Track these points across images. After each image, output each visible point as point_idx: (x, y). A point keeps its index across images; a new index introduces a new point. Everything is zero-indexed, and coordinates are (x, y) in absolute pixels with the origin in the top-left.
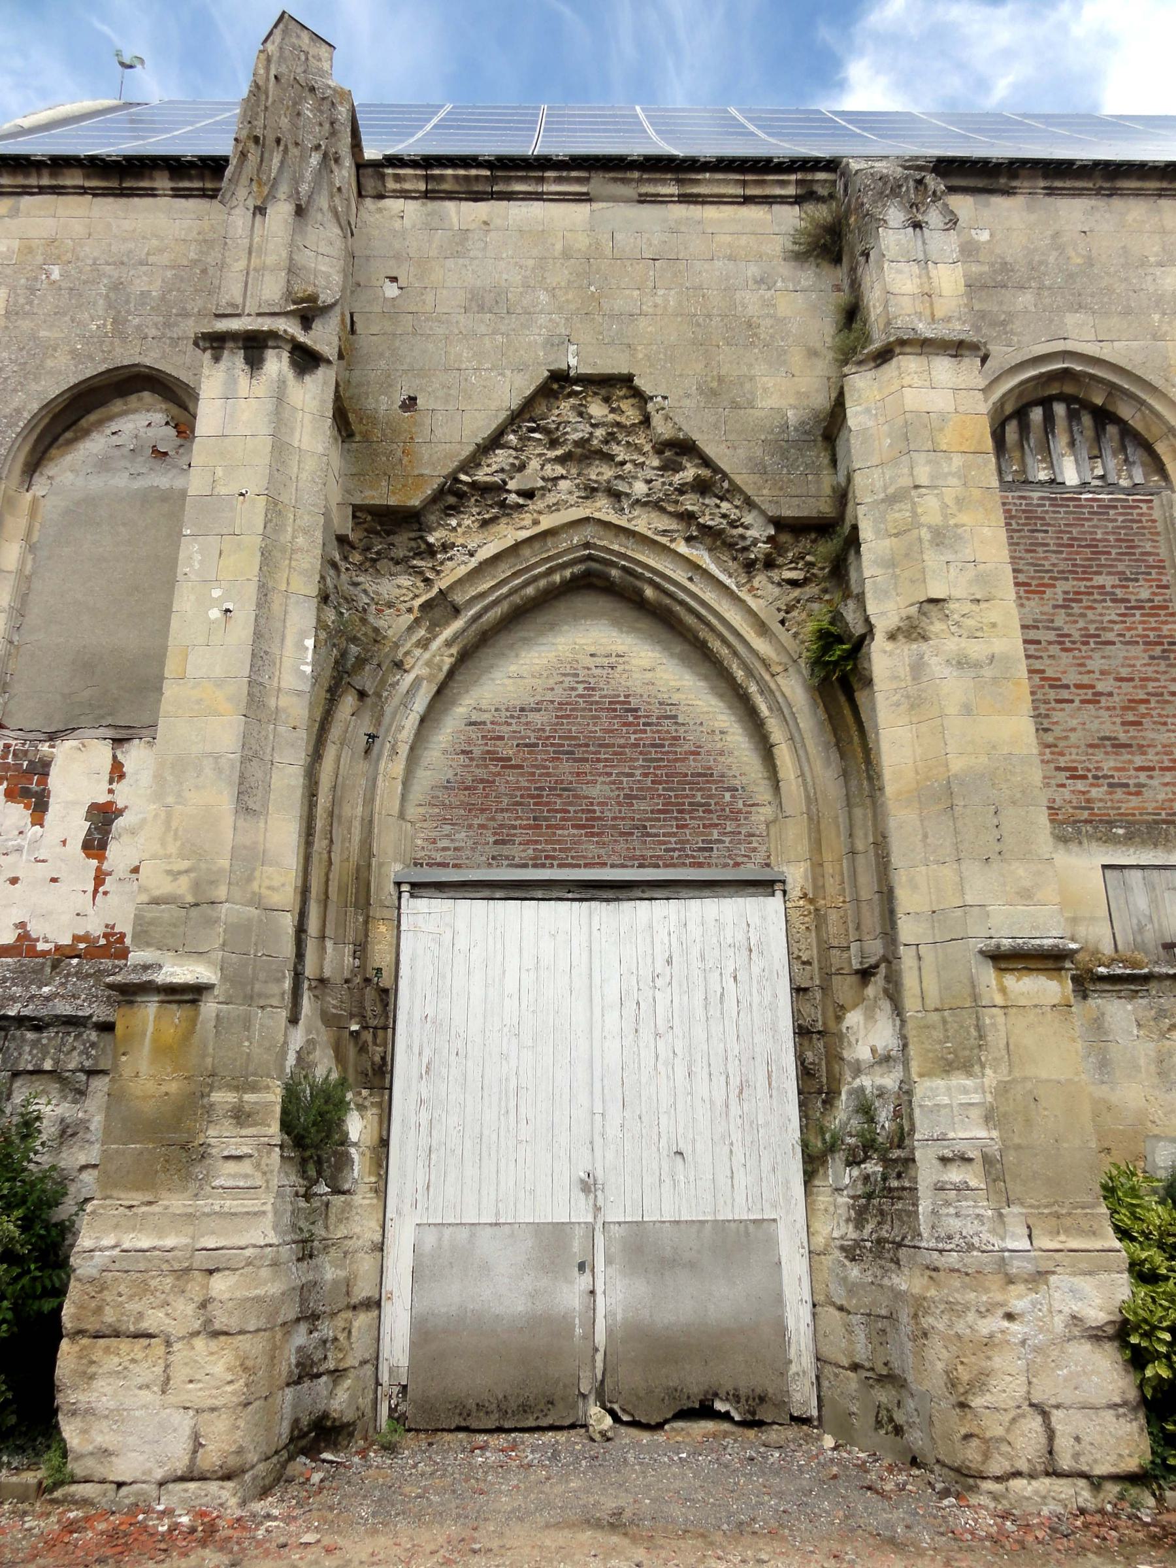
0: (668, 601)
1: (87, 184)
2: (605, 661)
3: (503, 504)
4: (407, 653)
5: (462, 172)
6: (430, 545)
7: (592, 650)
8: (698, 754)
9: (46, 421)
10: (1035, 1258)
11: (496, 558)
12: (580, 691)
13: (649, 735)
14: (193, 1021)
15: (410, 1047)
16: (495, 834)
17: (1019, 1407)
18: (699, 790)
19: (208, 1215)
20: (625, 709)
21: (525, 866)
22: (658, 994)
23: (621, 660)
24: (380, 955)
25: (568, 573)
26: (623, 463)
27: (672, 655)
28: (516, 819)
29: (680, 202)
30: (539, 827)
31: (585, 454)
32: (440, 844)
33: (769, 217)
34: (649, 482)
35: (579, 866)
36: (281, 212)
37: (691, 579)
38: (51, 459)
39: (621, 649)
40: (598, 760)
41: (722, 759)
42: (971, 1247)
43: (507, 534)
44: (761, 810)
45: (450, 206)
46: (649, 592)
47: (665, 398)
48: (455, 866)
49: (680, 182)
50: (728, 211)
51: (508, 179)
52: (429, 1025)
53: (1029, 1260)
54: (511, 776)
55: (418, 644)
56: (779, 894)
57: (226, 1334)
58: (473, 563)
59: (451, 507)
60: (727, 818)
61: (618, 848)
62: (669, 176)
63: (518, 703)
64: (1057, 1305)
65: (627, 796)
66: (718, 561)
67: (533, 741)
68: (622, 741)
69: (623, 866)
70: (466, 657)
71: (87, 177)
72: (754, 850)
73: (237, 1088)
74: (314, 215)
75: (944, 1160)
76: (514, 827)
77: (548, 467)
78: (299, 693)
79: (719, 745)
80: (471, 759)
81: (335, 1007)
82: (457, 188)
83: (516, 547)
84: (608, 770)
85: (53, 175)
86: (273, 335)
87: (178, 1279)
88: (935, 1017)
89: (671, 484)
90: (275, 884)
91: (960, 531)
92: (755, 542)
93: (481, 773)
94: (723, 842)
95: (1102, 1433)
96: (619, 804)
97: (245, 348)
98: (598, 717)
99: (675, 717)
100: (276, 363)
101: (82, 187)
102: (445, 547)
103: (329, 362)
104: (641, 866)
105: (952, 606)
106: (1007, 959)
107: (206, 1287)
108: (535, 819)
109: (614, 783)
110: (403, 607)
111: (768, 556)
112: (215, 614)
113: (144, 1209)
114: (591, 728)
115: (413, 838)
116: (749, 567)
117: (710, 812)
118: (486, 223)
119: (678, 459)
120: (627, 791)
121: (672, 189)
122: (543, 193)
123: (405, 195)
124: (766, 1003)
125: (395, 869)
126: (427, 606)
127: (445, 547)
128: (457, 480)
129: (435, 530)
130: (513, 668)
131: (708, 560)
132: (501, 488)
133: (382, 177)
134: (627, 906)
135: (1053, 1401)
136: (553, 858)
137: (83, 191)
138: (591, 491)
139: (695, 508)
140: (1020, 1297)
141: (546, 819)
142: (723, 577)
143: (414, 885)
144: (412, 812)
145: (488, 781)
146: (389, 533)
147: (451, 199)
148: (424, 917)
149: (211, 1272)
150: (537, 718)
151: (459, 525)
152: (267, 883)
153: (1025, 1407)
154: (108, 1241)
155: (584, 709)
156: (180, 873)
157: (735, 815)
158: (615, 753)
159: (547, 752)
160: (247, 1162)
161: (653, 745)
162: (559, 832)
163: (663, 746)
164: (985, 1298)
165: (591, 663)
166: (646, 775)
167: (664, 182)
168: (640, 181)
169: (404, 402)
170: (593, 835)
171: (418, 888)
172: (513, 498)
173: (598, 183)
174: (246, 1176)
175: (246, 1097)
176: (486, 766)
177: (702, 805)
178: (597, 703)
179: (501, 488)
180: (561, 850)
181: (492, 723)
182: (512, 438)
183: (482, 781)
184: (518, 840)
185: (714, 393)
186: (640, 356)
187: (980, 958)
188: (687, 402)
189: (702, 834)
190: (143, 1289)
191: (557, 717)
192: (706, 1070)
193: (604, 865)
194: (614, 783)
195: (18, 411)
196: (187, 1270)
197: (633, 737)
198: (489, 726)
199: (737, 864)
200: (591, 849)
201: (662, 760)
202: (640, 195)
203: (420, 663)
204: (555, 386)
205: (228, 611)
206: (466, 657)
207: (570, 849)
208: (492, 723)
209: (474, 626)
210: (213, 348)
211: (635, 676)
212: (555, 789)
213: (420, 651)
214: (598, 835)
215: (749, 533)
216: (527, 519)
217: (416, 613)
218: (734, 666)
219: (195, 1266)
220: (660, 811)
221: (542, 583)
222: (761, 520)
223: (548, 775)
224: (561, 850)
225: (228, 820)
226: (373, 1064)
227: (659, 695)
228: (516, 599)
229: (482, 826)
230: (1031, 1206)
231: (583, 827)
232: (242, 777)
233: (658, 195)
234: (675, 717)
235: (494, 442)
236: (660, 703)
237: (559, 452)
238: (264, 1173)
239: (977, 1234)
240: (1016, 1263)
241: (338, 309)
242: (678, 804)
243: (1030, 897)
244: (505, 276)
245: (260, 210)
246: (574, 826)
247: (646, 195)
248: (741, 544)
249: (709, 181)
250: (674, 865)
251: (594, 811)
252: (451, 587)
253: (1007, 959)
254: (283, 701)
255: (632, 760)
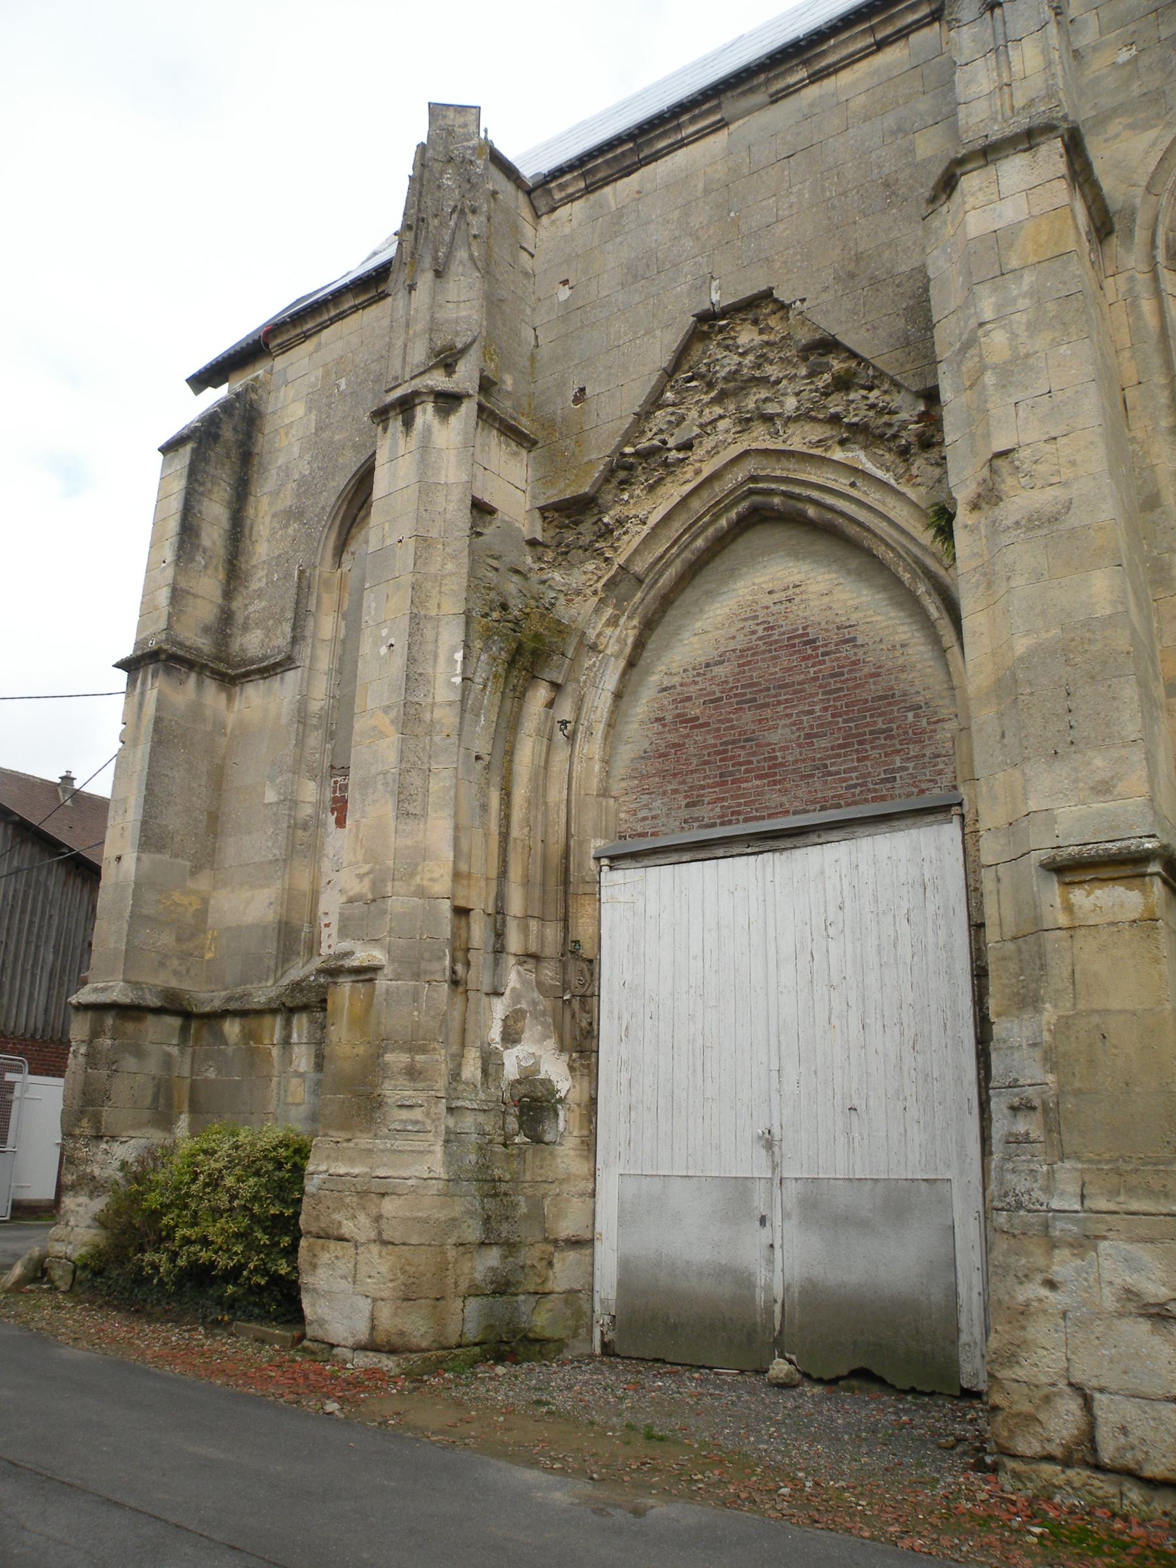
0: (829, 516)
1: (357, 302)
2: (781, 596)
3: (666, 464)
4: (599, 635)
5: (610, 156)
6: (606, 525)
7: (770, 587)
8: (878, 675)
9: (344, 507)
10: (1085, 1220)
11: (667, 518)
12: (760, 634)
13: (829, 664)
14: (371, 995)
15: (611, 1012)
16: (686, 797)
17: (1053, 1385)
18: (880, 715)
19: (382, 1151)
20: (803, 643)
21: (713, 825)
22: (832, 943)
23: (797, 590)
24: (582, 930)
25: (733, 514)
26: (778, 382)
27: (849, 572)
28: (705, 778)
29: (812, 82)
30: (724, 783)
31: (738, 385)
32: (640, 815)
33: (906, 52)
34: (797, 394)
35: (763, 818)
36: (425, 280)
37: (853, 485)
38: (353, 538)
39: (796, 578)
40: (779, 703)
41: (903, 676)
42: (1019, 1206)
43: (673, 492)
44: (947, 725)
45: (608, 190)
46: (811, 512)
47: (803, 300)
48: (653, 834)
49: (806, 63)
50: (862, 67)
51: (650, 142)
52: (626, 991)
53: (1076, 1222)
54: (698, 736)
55: (609, 623)
56: (956, 819)
57: (393, 1244)
58: (646, 529)
59: (622, 482)
60: (909, 741)
61: (800, 793)
62: (794, 62)
63: (702, 659)
64: (1106, 1276)
65: (808, 736)
66: (874, 458)
67: (718, 695)
68: (802, 677)
69: (806, 811)
70: (649, 626)
71: (356, 296)
72: (940, 772)
73: (410, 1050)
74: (456, 268)
75: (1014, 1109)
76: (703, 787)
77: (707, 411)
78: (451, 704)
79: (900, 661)
80: (664, 726)
81: (552, 979)
82: (609, 172)
83: (685, 500)
84: (789, 711)
85: (336, 305)
86: (416, 394)
87: (361, 1198)
88: (1011, 946)
89: (816, 391)
90: (435, 875)
91: (1031, 361)
92: (904, 425)
93: (672, 738)
94: (906, 769)
95: (1156, 1429)
96: (800, 746)
97: (402, 412)
98: (777, 657)
99: (854, 639)
100: (425, 414)
101: (355, 306)
102: (620, 522)
103: (469, 396)
104: (823, 809)
105: (1024, 454)
106: (1069, 869)
107: (379, 1206)
108: (721, 775)
109: (794, 724)
110: (589, 592)
111: (920, 436)
112: (384, 650)
113: (345, 1144)
114: (773, 670)
115: (617, 812)
116: (904, 453)
117: (891, 737)
118: (639, 192)
119: (824, 359)
120: (807, 731)
121: (802, 73)
122: (683, 139)
123: (571, 199)
124: (941, 944)
125: (596, 844)
126: (611, 584)
127: (620, 522)
128: (623, 455)
129: (610, 508)
130: (698, 624)
131: (864, 460)
132: (664, 446)
133: (549, 191)
134: (798, 854)
135: (1094, 1383)
136: (739, 813)
137: (356, 309)
138: (745, 423)
139: (839, 409)
140: (1063, 1263)
141: (732, 774)
142: (880, 474)
143: (612, 858)
144: (617, 787)
145: (678, 745)
146: (577, 523)
147: (607, 184)
148: (619, 886)
149: (383, 1195)
150: (719, 671)
151: (631, 497)
152: (428, 875)
153: (1062, 1385)
154: (322, 1168)
155: (764, 652)
156: (364, 875)
157: (918, 736)
158: (795, 692)
159: (731, 704)
160: (418, 1111)
161: (833, 676)
162: (744, 785)
163: (842, 674)
164: (1023, 1262)
165: (768, 600)
166: (825, 709)
167: (790, 71)
168: (768, 81)
169: (575, 396)
170: (775, 783)
171: (615, 860)
172: (674, 455)
173: (730, 105)
174: (417, 1122)
175: (417, 1057)
176: (677, 730)
177: (882, 731)
178: (776, 641)
179: (664, 446)
180: (746, 804)
181: (681, 685)
182: (669, 395)
183: (674, 745)
184: (706, 800)
185: (852, 276)
186: (778, 265)
187: (1041, 871)
188: (825, 296)
189: (885, 763)
190: (341, 1205)
191: (739, 665)
192: (879, 1023)
193: (787, 812)
194: (794, 724)
195: (323, 508)
196: (367, 1192)
197: (812, 670)
198: (679, 688)
199: (922, 791)
200: (774, 798)
201: (841, 689)
202: (771, 96)
203: (612, 641)
204: (705, 328)
205: (392, 645)
206: (649, 626)
207: (754, 801)
208: (681, 685)
209: (652, 593)
210: (383, 421)
211: (812, 604)
212: (739, 741)
213: (611, 629)
214: (780, 782)
215: (895, 418)
216: (689, 471)
217: (601, 594)
218: (900, 570)
219: (373, 1189)
220: (841, 746)
221: (711, 531)
222: (909, 399)
223: (732, 728)
224: (746, 804)
225: (392, 824)
226: (581, 1030)
227: (838, 620)
228: (687, 555)
229: (675, 791)
230: (1090, 1161)
231: (766, 776)
232: (401, 786)
233: (789, 87)
234: (854, 639)
235: (655, 402)
236: (838, 628)
237: (713, 394)
238: (434, 1121)
239: (1029, 1192)
240: (1059, 1225)
241: (476, 345)
242: (859, 735)
243: (1108, 791)
244: (654, 238)
245: (411, 288)
246: (758, 777)
247: (777, 92)
248: (890, 432)
249: (835, 47)
250: (854, 803)
251: (776, 758)
252: (628, 560)
253: (1069, 869)
254: (437, 714)
255: (812, 695)
